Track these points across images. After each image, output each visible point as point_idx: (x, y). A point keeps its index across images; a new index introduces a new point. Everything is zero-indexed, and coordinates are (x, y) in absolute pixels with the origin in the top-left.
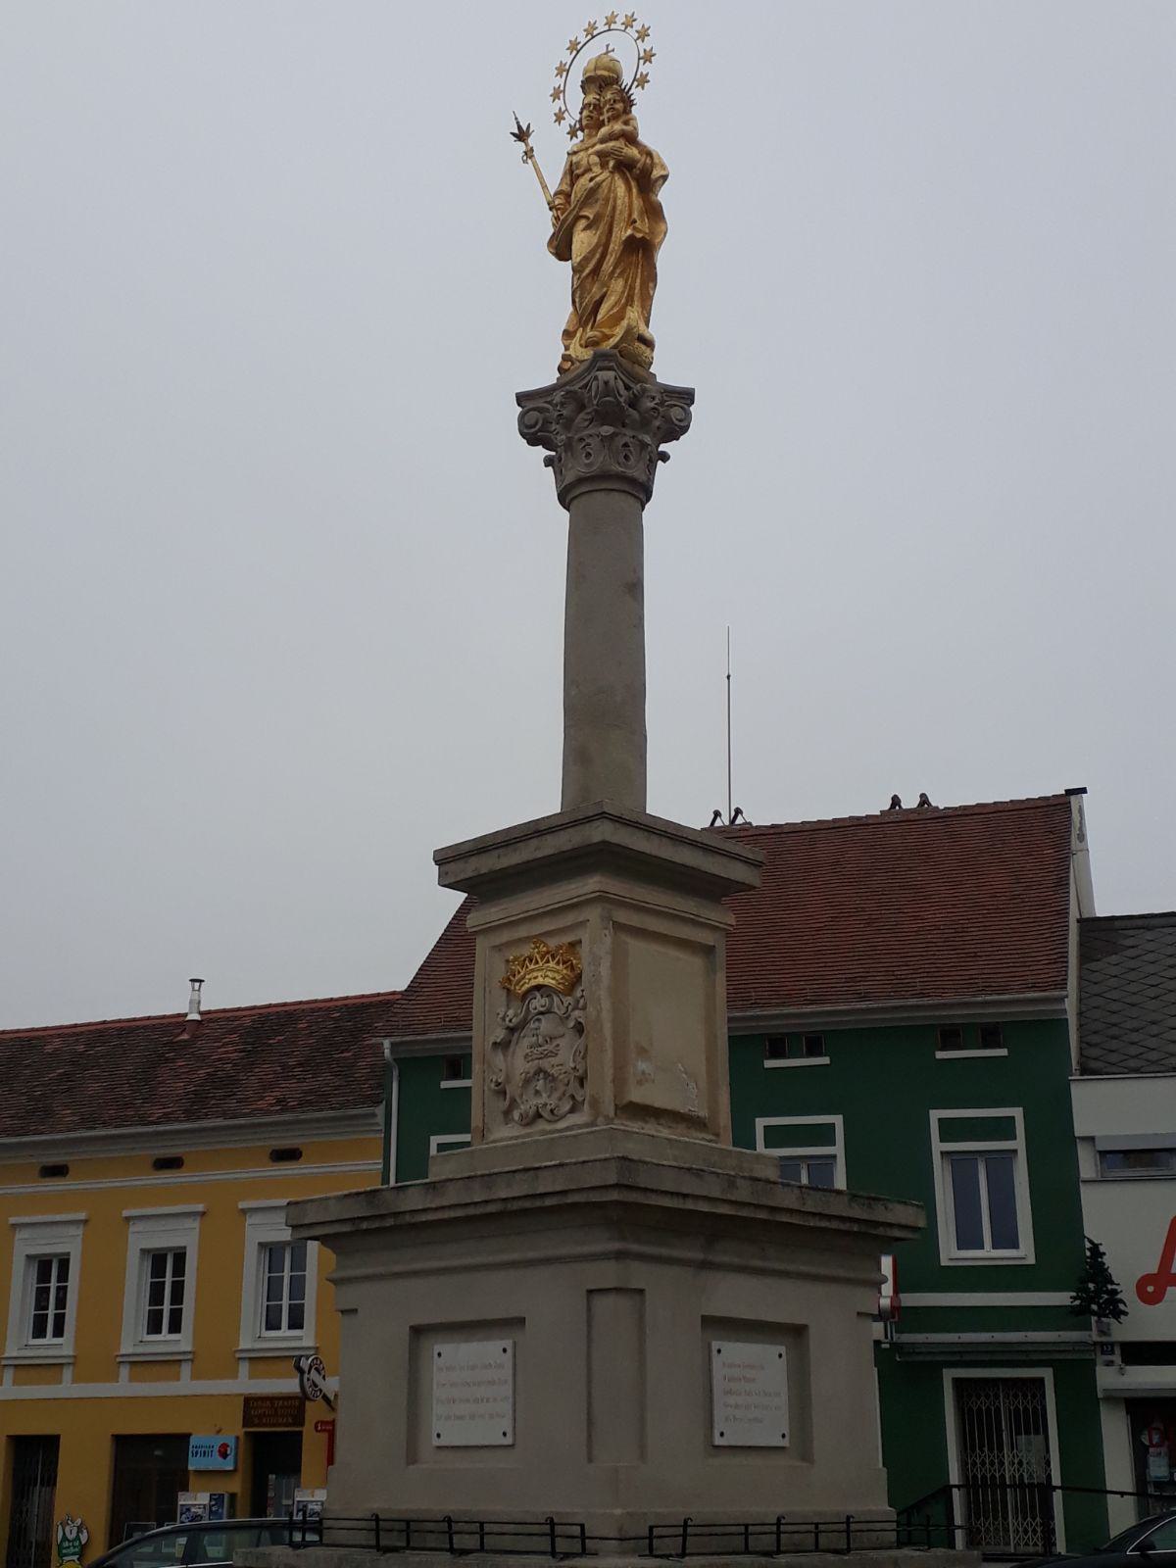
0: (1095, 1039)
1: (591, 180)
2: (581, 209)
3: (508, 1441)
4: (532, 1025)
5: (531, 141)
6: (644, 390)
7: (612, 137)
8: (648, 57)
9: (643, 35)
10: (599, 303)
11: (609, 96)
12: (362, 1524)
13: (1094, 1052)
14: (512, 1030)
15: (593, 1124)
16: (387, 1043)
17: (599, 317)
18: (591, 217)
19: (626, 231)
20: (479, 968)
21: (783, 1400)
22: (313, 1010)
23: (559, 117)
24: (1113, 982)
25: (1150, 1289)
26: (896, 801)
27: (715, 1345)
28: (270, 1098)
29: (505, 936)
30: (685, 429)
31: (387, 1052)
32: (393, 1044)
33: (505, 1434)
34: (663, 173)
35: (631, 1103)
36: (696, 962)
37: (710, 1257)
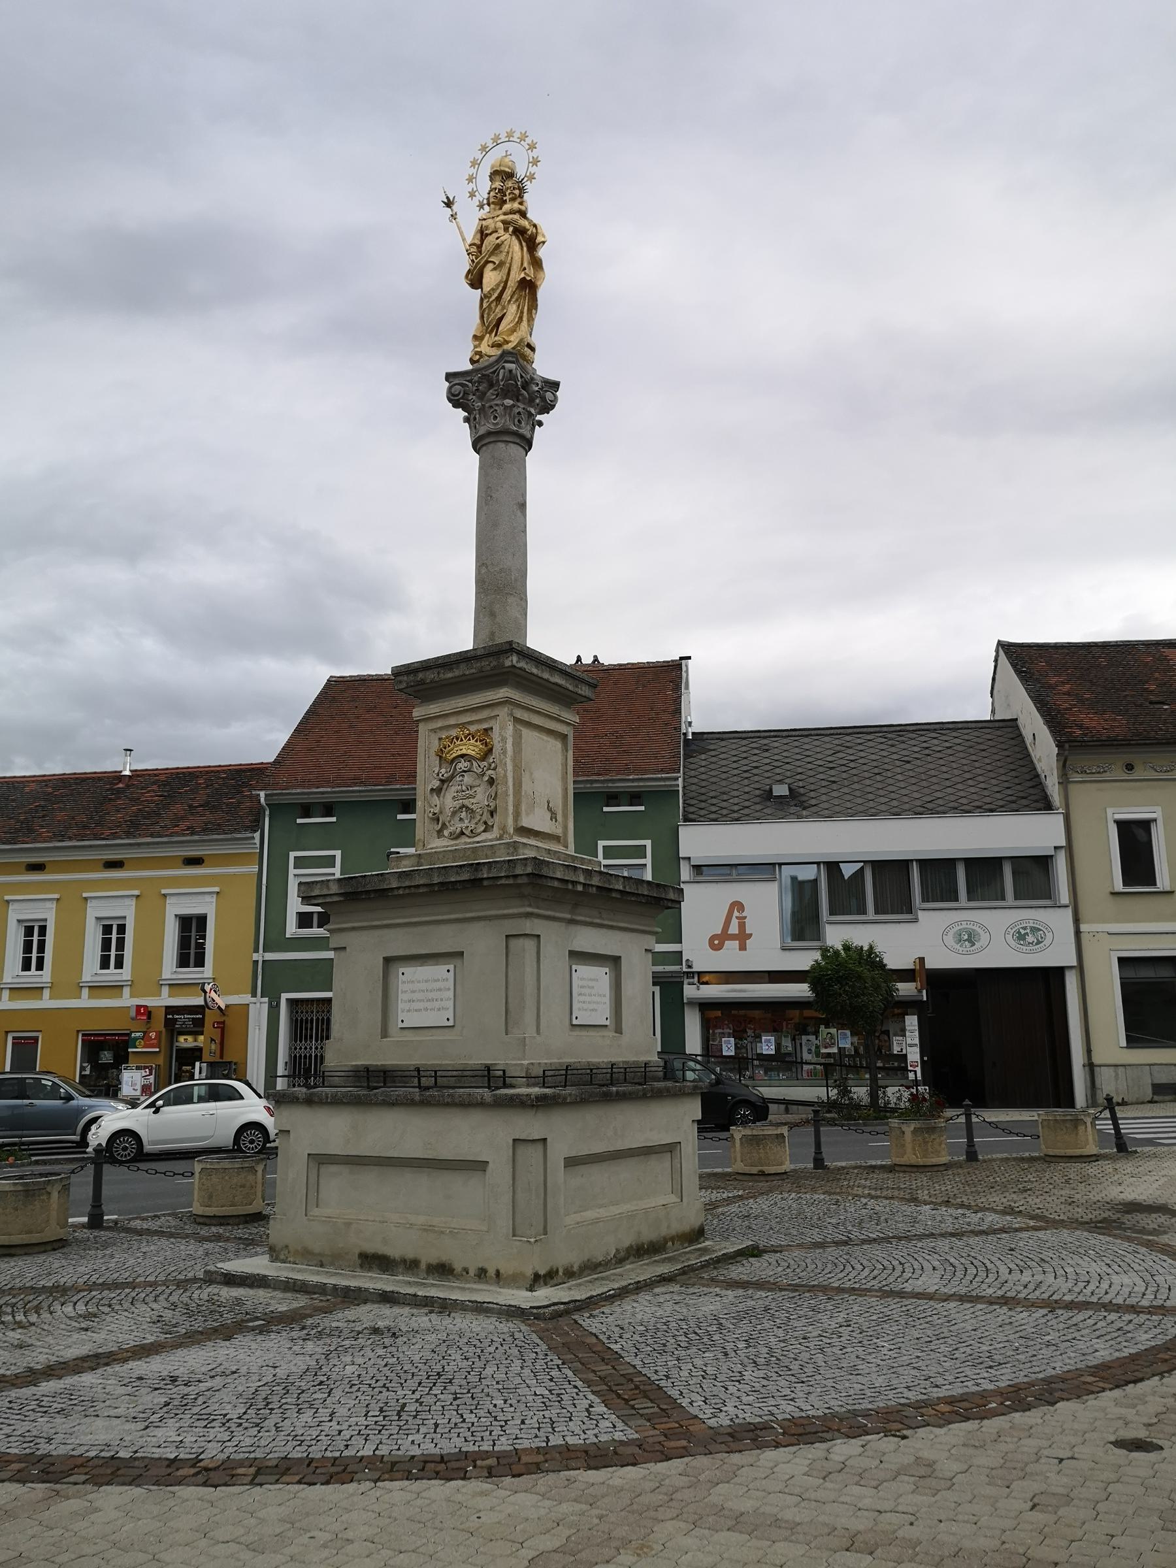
0: (693, 802)
1: (498, 238)
2: (489, 257)
3: (451, 1023)
4: (458, 778)
5: (454, 207)
6: (532, 379)
7: (512, 212)
8: (535, 162)
9: (532, 147)
10: (501, 319)
11: (510, 185)
12: (350, 1074)
13: (692, 809)
14: (442, 781)
15: (501, 838)
16: (262, 794)
17: (500, 329)
18: (497, 263)
19: (519, 275)
20: (421, 743)
21: (607, 999)
22: (207, 772)
23: (472, 195)
24: (703, 769)
25: (716, 942)
26: (579, 659)
27: (574, 967)
28: (183, 825)
29: (440, 724)
30: (553, 407)
31: (262, 800)
32: (266, 795)
33: (448, 1019)
34: (543, 239)
35: (522, 827)
36: (558, 745)
37: (574, 917)
